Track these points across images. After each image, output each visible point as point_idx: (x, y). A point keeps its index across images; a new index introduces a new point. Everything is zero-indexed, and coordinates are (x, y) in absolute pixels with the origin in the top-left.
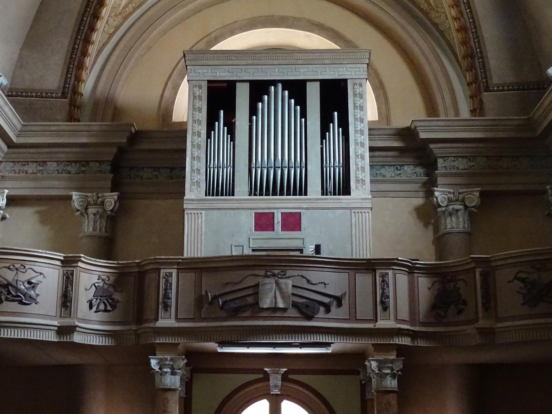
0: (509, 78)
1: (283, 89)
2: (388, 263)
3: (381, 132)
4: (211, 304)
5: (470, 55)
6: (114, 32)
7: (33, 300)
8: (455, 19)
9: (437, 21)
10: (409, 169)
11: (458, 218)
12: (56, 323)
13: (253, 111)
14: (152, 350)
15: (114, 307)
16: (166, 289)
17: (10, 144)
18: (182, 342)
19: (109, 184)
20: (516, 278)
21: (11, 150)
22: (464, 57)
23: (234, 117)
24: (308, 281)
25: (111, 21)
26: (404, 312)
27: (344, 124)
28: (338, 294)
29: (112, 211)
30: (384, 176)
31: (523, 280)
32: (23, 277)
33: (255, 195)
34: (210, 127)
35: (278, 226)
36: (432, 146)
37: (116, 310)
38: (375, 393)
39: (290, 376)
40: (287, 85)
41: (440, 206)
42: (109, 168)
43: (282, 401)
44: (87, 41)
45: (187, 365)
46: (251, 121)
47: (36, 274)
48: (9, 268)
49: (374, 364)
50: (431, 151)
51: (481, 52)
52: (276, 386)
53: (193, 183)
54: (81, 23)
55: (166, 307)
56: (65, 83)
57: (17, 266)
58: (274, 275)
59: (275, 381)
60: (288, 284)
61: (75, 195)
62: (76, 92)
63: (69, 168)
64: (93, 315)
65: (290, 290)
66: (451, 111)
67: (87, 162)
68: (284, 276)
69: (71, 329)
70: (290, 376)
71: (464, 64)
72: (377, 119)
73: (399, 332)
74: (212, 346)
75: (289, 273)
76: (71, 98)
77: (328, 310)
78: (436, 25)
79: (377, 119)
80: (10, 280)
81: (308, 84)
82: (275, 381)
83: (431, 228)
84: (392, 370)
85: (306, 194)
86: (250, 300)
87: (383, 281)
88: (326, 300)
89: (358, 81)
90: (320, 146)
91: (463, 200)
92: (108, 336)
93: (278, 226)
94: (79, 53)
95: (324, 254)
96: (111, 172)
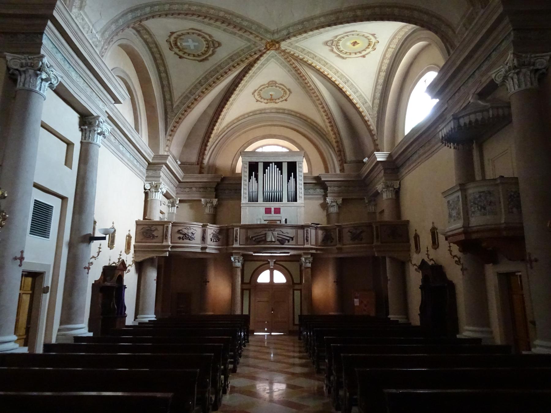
0: (353, 158)
1: (275, 165)
2: (308, 226)
3: (309, 178)
4: (251, 239)
5: (339, 151)
6: (215, 142)
7: (193, 239)
8: (334, 138)
9: (329, 138)
10: (318, 190)
11: (334, 208)
12: (200, 246)
13: (264, 172)
14: (232, 254)
15: (219, 240)
16: (236, 235)
17: (180, 182)
18: (241, 252)
19: (214, 196)
20: (349, 232)
21: (180, 184)
23: (258, 172)
24: (282, 232)
25: (214, 138)
26: (313, 242)
27: (295, 177)
28: (292, 236)
29: (215, 205)
30: (310, 193)
31: (351, 232)
32: (190, 231)
33: (265, 202)
34: (250, 178)
35: (273, 212)
36: (326, 183)
37: (220, 241)
39: (277, 262)
40: (276, 163)
41: (328, 204)
42: (214, 190)
43: (257, 282)
44: (206, 145)
45: (243, 259)
46: (264, 176)
47: (194, 230)
48: (185, 228)
49: (303, 259)
50: (326, 184)
52: (272, 266)
53: (244, 198)
55: (236, 240)
56: (198, 159)
57: (188, 228)
58: (271, 230)
59: (272, 264)
60: (276, 233)
61: (203, 200)
63: (200, 190)
64: (212, 243)
65: (277, 235)
66: (333, 170)
67: (207, 188)
68: (274, 231)
69: (205, 248)
70: (277, 262)
71: (338, 153)
72: (307, 172)
73: (312, 249)
74: (251, 253)
75: (276, 229)
76: (200, 166)
77: (289, 242)
79: (307, 172)
80: (186, 232)
81: (283, 163)
82: (272, 264)
83: (326, 211)
84: (309, 261)
85: (282, 201)
86: (264, 238)
87: (307, 232)
88: (288, 238)
89: (300, 162)
90: (287, 185)
91: (336, 202)
92: (216, 250)
93: (273, 212)
94: (203, 150)
95: (288, 223)
96: (215, 191)
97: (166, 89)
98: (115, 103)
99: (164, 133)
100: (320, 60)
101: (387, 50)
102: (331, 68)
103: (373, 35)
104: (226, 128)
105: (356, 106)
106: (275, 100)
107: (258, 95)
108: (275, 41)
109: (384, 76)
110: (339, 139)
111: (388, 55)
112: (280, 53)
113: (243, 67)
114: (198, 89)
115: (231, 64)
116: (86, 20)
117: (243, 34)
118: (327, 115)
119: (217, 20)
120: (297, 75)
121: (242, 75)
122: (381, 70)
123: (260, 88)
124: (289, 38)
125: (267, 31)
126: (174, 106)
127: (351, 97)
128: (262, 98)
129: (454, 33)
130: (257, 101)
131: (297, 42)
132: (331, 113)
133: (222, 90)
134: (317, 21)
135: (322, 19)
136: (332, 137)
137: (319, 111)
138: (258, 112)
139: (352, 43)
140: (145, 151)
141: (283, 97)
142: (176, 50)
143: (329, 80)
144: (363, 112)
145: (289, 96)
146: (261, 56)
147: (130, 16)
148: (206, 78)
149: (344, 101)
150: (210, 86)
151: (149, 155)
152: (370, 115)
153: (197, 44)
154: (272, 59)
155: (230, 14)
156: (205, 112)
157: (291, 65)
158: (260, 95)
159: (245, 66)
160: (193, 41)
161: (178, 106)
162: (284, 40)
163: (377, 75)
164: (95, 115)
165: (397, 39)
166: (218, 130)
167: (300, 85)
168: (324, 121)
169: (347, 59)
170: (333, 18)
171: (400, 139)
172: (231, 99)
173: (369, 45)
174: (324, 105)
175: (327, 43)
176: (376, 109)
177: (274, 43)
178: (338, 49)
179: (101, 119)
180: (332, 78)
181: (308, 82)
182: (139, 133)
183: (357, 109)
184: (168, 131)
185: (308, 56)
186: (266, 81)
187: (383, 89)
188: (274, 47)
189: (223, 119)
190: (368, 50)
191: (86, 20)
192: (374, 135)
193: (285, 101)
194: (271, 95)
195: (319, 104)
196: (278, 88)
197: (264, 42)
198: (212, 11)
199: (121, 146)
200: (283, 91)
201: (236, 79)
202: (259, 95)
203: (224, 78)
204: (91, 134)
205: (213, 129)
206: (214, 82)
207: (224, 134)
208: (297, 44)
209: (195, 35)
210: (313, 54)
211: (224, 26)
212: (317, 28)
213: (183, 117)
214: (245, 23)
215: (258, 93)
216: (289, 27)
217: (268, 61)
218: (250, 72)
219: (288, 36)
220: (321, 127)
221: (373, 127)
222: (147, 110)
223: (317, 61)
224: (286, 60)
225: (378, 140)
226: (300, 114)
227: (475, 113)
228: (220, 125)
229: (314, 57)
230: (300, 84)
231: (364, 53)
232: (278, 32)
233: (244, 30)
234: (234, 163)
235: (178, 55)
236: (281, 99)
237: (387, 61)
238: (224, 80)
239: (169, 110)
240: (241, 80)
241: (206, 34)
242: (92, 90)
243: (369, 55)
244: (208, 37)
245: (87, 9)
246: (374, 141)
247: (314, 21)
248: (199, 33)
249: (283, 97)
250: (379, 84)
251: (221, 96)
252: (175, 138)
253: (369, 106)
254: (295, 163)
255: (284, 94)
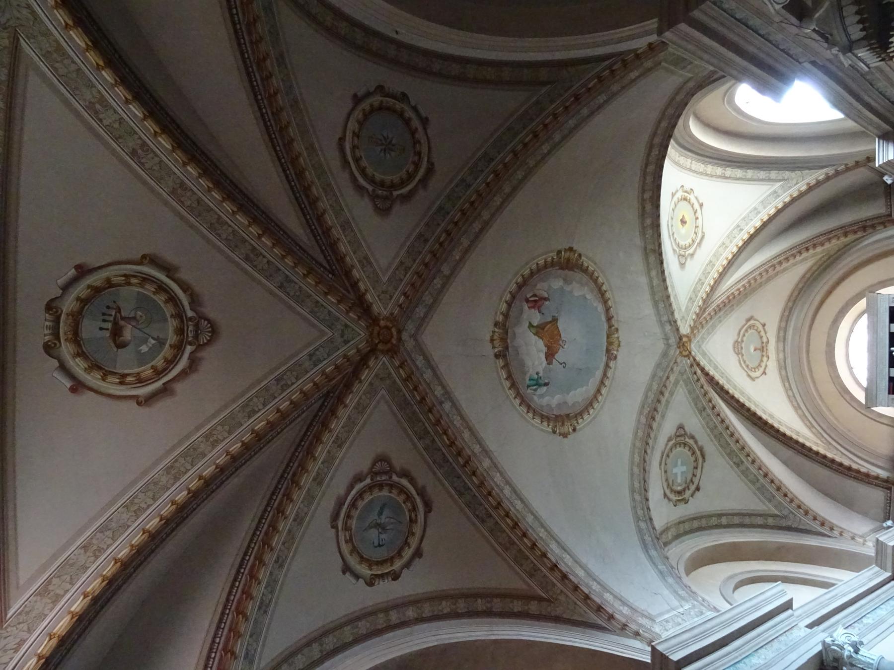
5: (864, 228)
22: (865, 231)
38: (595, 305)
44: (849, 469)
51: (862, 222)
54: (836, 471)
62: (886, 481)
78: (839, 250)
81: (891, 331)
94: (858, 475)
97: (747, 521)
98: (792, 609)
99: (826, 538)
100: (706, 274)
101: (695, 172)
102: (717, 255)
103: (673, 195)
104: (814, 430)
105: (780, 209)
106: (763, 343)
107: (755, 371)
108: (679, 343)
109: (731, 169)
110: (840, 232)
111: (700, 167)
112: (695, 335)
113: (716, 395)
114: (747, 469)
115: (709, 411)
116: (666, 616)
117: (669, 389)
118: (794, 256)
119: (651, 427)
120: (726, 308)
121: (726, 396)
122: (723, 175)
123: (744, 367)
124: (675, 322)
125: (665, 354)
126: (777, 512)
127: (766, 218)
128: (760, 365)
129: (690, 79)
130: (764, 373)
131: (680, 310)
132: (791, 249)
133: (748, 429)
134: (655, 282)
135: (653, 273)
136: (834, 245)
137: (785, 270)
138: (783, 373)
139: (683, 226)
140: (871, 580)
141: (759, 330)
142: (688, 493)
143: (736, 256)
144: (791, 196)
145: (757, 321)
146: (698, 365)
147: (653, 553)
148: (731, 454)
149: (772, 228)
150: (743, 448)
151: (877, 575)
152: (797, 183)
153: (679, 462)
154: (703, 346)
155: (643, 407)
156: (785, 463)
157: (711, 318)
158: (754, 368)
159: (712, 390)
160: (676, 465)
161: (775, 507)
162: (678, 330)
163: (730, 181)
164: (819, 648)
165: (679, 159)
166: (817, 443)
167: (741, 303)
168: (806, 259)
169: (704, 231)
170: (652, 258)
171: (851, 124)
172: (764, 417)
173: (685, 199)
174: (775, 262)
175: (682, 264)
176: (787, 174)
177: (681, 344)
178: (690, 246)
179: (828, 640)
180: (732, 253)
181: (739, 289)
182: (833, 585)
183: (786, 206)
184: (823, 531)
185: (699, 291)
186: (733, 359)
187: (740, 167)
188: (686, 345)
189: (798, 433)
190: (693, 200)
191: (666, 616)
192: (836, 170)
193: (765, 327)
194: (755, 350)
195: (774, 270)
196: (745, 339)
197: (679, 360)
198: (640, 434)
199: (865, 620)
200: (749, 330)
201: (731, 406)
202: (754, 369)
203: (730, 424)
204: (859, 666)
205: (817, 453)
206: (737, 441)
207: (825, 435)
208: (683, 309)
209: (669, 461)
210: (697, 284)
211: (658, 417)
212: (664, 280)
213: (796, 501)
214: (655, 387)
215: (753, 370)
216: (661, 321)
217: (706, 354)
218: (721, 382)
219: (673, 323)
220: (815, 264)
221: (820, 174)
222: (782, 559)
223: (706, 278)
224: (704, 326)
225: (846, 162)
226: (789, 300)
227: (842, 18)
228: (808, 439)
229: (701, 282)
230: (739, 303)
231: (697, 206)
232: (667, 339)
233: (664, 389)
234: (886, 422)
235: (694, 492)
236: (763, 333)
237: (710, 169)
238: (733, 426)
239: (784, 523)
240: (733, 397)
241: (667, 445)
242: (775, 640)
243: (699, 198)
244: (671, 443)
245: (653, 612)
246: (848, 169)
247: (654, 285)
248: (665, 455)
249: (759, 330)
250: (724, 173)
251: (755, 429)
252: (835, 522)
253: (782, 186)
254: (892, 309)
255: (753, 329)
